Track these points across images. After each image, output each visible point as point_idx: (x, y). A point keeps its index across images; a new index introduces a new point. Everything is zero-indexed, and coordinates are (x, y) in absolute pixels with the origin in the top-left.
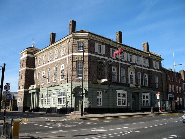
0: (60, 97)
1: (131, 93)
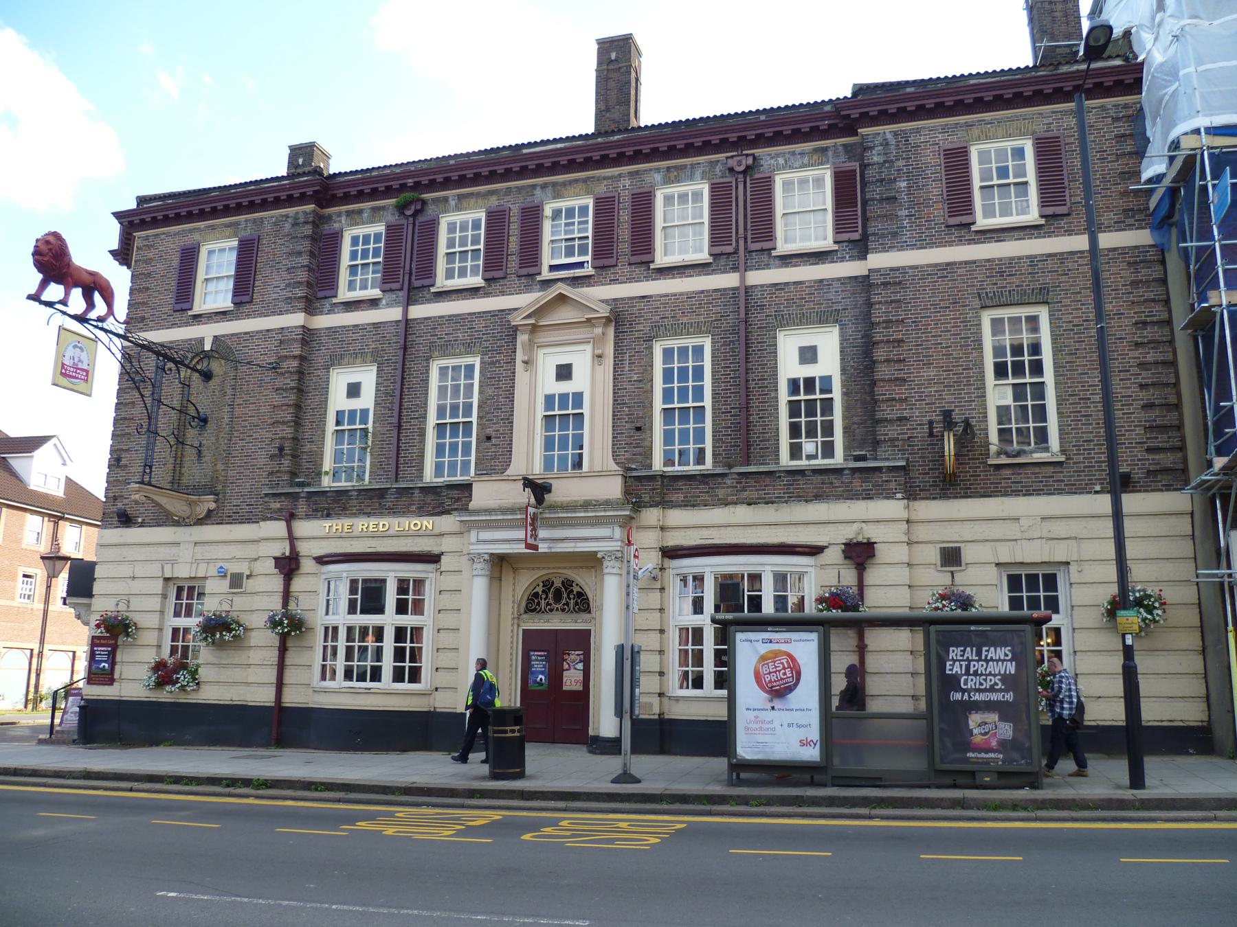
0: (340, 664)
1: (480, 567)
